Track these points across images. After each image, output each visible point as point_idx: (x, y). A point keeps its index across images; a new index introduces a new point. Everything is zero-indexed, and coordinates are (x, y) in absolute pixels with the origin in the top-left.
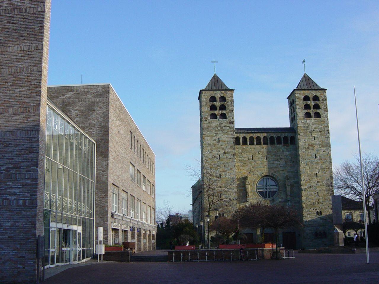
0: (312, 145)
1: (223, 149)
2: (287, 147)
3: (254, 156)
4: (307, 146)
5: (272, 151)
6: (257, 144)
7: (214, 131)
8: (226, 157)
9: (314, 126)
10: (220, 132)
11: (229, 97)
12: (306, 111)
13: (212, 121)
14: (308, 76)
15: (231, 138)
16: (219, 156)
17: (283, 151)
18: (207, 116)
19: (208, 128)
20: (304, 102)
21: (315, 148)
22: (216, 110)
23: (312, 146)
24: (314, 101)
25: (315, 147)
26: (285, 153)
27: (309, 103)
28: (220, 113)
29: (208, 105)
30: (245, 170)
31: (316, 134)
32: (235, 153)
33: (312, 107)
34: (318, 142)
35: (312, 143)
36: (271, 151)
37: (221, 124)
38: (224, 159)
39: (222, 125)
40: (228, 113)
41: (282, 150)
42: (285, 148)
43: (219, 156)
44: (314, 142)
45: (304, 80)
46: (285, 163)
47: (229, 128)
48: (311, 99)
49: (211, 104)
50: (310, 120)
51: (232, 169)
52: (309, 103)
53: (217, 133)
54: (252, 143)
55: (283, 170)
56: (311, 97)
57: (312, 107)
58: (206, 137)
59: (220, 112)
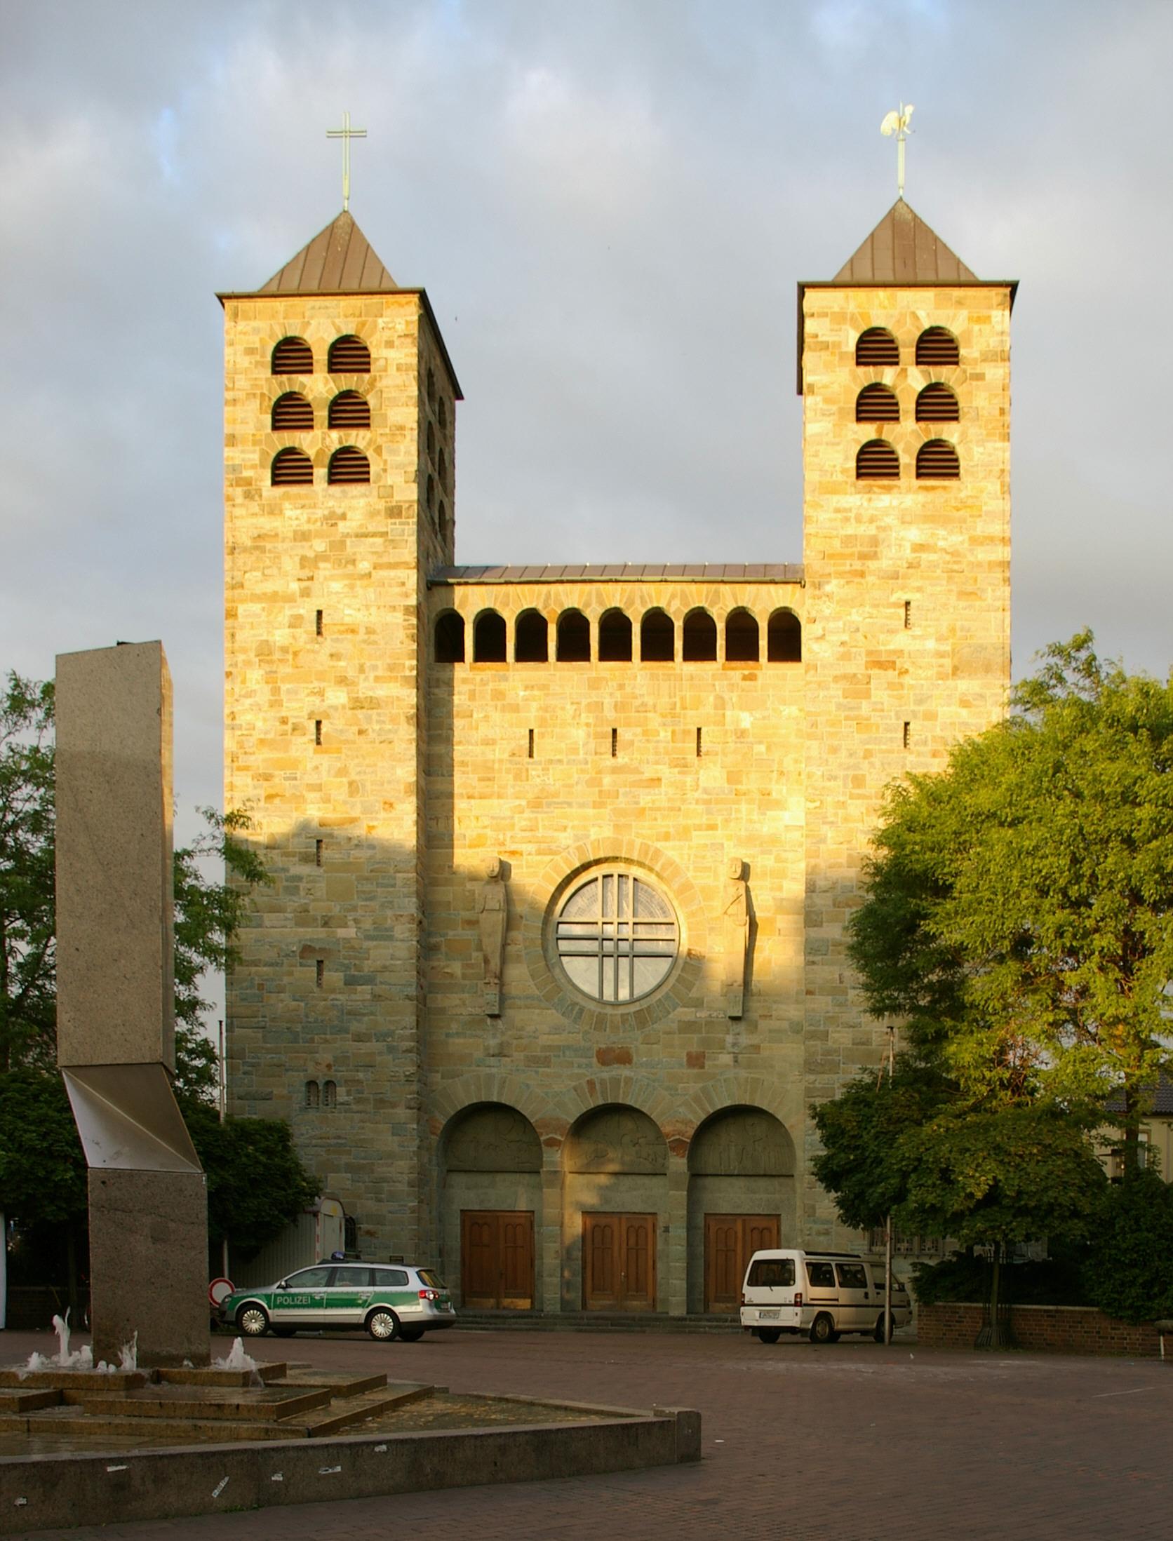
0: (882, 663)
1: (342, 681)
2: (745, 678)
3: (542, 735)
4: (857, 667)
5: (650, 701)
6: (563, 656)
7: (290, 565)
8: (360, 732)
9: (914, 534)
10: (327, 573)
11: (390, 344)
12: (868, 432)
13: (286, 497)
14: (915, 217)
15: (394, 608)
16: (318, 723)
17: (721, 704)
18: (253, 467)
19: (257, 548)
20: (862, 369)
21: (907, 680)
22: (306, 424)
23: (892, 665)
24: (922, 367)
25: (907, 671)
26: (728, 719)
27: (887, 376)
28: (336, 446)
29: (263, 395)
30: (487, 822)
31: (919, 589)
32: (1152, 951)
33: (907, 405)
34: (931, 644)
35: (892, 647)
36: (644, 704)
37: (333, 519)
38: (347, 742)
39: (343, 527)
40: (379, 450)
41: (711, 699)
42: (732, 687)
43: (318, 723)
44: (901, 640)
45: (887, 235)
46: (729, 781)
47: (379, 540)
48: (907, 353)
49: (281, 384)
50: (888, 489)
51: (391, 805)
52: (887, 376)
53: (311, 578)
54: (531, 649)
55: (712, 827)
56: (906, 337)
57: (907, 405)
58: (242, 601)
59: (335, 440)
